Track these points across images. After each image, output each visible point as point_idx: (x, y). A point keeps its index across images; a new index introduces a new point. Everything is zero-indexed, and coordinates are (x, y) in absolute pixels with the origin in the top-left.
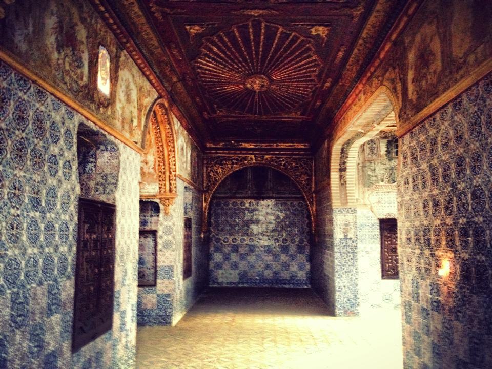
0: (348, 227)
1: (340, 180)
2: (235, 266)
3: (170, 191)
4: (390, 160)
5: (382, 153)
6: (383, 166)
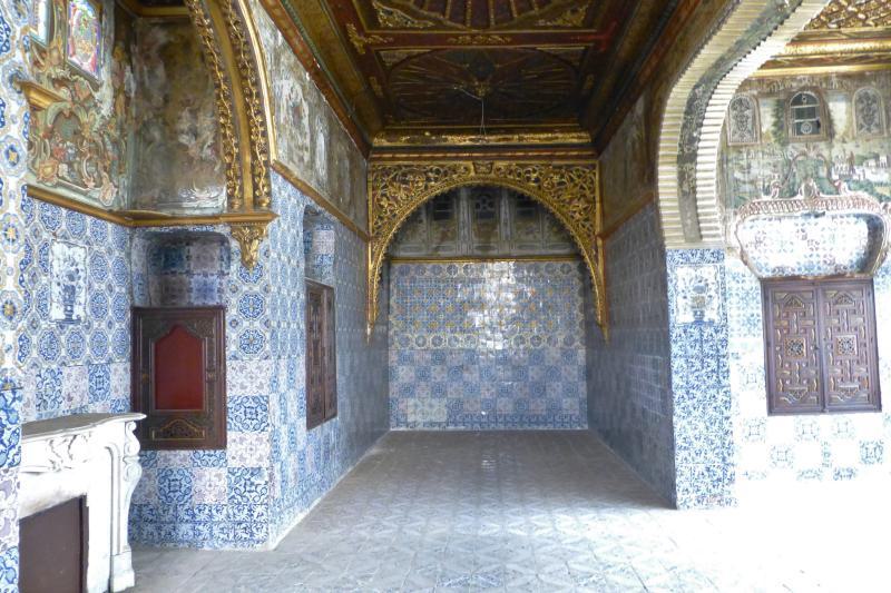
0: (703, 295)
1: (681, 185)
2: (438, 391)
3: (256, 202)
4: (784, 143)
5: (764, 130)
6: (767, 159)
